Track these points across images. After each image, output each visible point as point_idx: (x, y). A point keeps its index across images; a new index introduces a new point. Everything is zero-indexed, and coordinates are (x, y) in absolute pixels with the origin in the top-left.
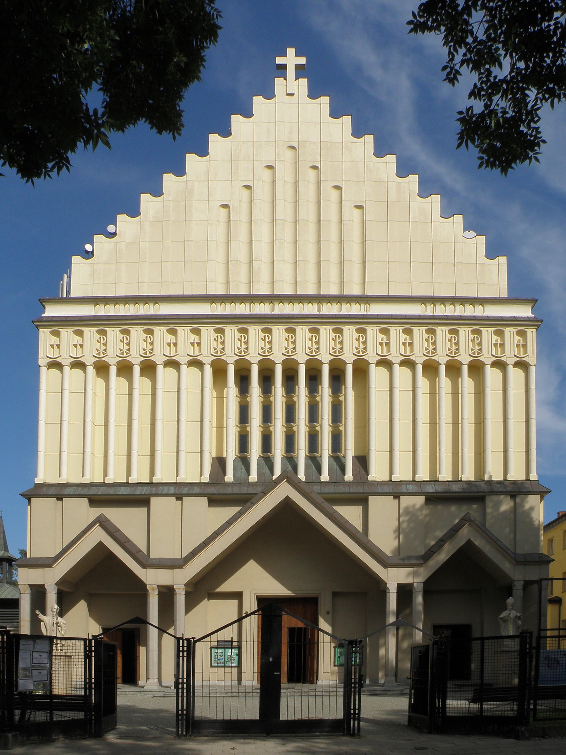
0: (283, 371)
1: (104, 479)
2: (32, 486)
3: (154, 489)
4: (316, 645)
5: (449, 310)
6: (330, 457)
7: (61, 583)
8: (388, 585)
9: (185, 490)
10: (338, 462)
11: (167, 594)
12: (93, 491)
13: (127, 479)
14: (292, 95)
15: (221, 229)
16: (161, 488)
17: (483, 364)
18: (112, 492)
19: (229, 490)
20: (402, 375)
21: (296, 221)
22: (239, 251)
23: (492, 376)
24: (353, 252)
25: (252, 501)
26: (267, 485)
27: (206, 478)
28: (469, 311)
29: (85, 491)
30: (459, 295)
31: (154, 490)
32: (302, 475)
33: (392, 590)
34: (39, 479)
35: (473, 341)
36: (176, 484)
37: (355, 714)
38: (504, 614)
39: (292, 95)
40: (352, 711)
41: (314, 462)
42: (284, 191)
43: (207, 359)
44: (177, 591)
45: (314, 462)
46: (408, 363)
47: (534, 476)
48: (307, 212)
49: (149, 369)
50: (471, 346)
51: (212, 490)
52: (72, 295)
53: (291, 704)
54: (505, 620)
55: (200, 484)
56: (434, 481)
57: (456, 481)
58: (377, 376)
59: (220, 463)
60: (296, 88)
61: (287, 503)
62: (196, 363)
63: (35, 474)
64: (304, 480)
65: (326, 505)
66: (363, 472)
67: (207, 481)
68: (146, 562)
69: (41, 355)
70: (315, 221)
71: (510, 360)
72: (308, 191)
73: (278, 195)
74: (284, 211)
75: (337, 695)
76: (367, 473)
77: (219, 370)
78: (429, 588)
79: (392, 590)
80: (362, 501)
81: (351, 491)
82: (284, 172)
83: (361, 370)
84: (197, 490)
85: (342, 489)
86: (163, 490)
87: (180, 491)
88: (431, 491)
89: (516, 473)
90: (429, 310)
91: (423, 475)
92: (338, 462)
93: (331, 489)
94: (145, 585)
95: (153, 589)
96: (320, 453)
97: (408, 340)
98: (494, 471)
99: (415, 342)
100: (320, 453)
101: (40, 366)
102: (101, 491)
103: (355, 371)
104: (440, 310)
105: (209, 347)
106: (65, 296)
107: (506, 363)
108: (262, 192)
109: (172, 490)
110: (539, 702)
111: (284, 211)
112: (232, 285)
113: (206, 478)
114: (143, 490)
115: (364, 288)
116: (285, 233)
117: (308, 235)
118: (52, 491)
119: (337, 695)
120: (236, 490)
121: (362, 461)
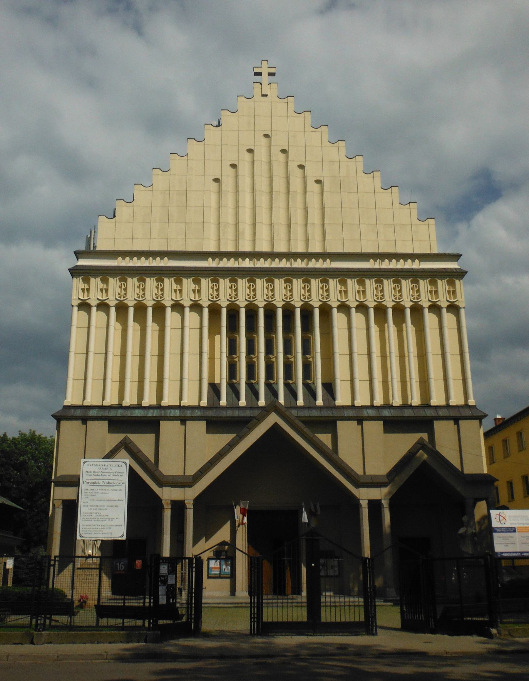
0: (246, 312)
1: (180, 403)
2: (61, 408)
3: (163, 412)
4: (518, 563)
5: (394, 265)
6: (246, 383)
7: (197, 501)
8: (361, 501)
9: (189, 413)
10: (310, 391)
11: (178, 507)
12: (112, 413)
13: (180, 403)
14: (266, 96)
15: (214, 197)
16: (169, 411)
17: (331, 308)
18: (129, 415)
19: (224, 414)
20: (358, 318)
21: (271, 192)
22: (228, 217)
23: (430, 320)
24: (314, 217)
25: (249, 425)
26: (266, 411)
27: (204, 402)
28: (409, 265)
29: (106, 413)
30: (135, 249)
31: (163, 413)
32: (281, 400)
33: (364, 504)
34: (69, 401)
35: (412, 289)
36: (180, 407)
37: (254, 622)
38: (462, 531)
39: (266, 96)
40: (256, 620)
41: (291, 391)
42: (262, 168)
43: (205, 303)
44: (188, 506)
45: (291, 391)
46: (362, 308)
47: (472, 402)
48: (279, 185)
49: (159, 309)
50: (393, 293)
51: (211, 413)
52: (98, 248)
53: (352, 616)
54: (463, 536)
55: (199, 407)
56: (387, 406)
57: (406, 406)
58: (338, 319)
59: (214, 388)
60: (269, 90)
61: (275, 427)
62: (196, 307)
63: (65, 398)
64: (283, 404)
65: (306, 430)
66: (216, 398)
67: (206, 405)
68: (359, 483)
69: (74, 297)
70: (285, 191)
71: (353, 304)
72: (279, 170)
73: (257, 172)
74: (262, 184)
75: (278, 606)
76: (334, 399)
77: (215, 311)
78: (395, 502)
79: (364, 504)
80: (329, 424)
81: (323, 415)
82: (261, 155)
83: (326, 311)
84: (197, 413)
85: (236, 413)
86: (170, 413)
87: (184, 415)
88: (387, 415)
89: (456, 400)
90: (143, 262)
91: (111, 400)
92: (310, 391)
93: (306, 413)
94: (161, 500)
95: (167, 503)
96: (275, 381)
97: (343, 289)
98: (437, 399)
99: (367, 290)
100: (275, 381)
101: (72, 306)
102: (119, 413)
103: (210, 312)
104: (386, 265)
105: (189, 289)
106: (92, 249)
107: (368, 306)
108: (244, 169)
109: (177, 413)
110: (142, 605)
111: (262, 184)
112: (240, 242)
113: (204, 402)
114: (153, 412)
115: (324, 246)
116: (263, 200)
117: (280, 202)
118: (78, 413)
119: (278, 606)
120: (230, 413)
121: (329, 388)
